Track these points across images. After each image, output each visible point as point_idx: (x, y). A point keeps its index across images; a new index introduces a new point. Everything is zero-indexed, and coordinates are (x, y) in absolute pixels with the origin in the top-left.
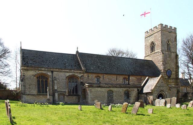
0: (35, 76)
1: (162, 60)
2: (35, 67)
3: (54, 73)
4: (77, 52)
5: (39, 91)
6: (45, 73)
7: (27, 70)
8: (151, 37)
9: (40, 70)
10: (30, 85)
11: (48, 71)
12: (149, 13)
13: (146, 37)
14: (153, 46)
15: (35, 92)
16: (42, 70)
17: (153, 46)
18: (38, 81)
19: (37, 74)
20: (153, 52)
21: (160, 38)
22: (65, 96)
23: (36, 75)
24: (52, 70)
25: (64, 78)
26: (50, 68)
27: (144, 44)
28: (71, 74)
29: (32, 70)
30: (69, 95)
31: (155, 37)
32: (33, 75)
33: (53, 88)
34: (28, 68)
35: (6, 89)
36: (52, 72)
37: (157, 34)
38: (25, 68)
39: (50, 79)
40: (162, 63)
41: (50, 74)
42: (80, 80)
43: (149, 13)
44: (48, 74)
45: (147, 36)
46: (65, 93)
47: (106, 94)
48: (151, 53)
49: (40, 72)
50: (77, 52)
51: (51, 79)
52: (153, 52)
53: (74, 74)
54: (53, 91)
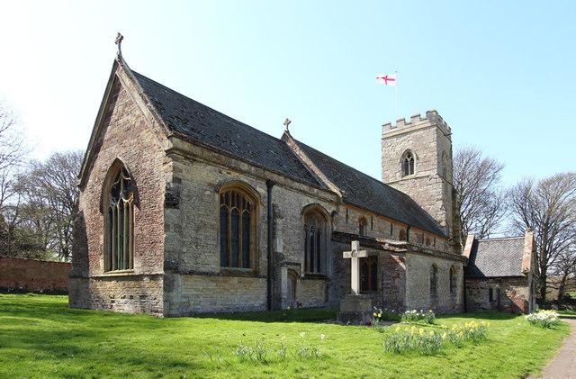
0: (216, 188)
1: (441, 197)
2: (219, 152)
3: (275, 188)
4: (287, 135)
5: (225, 261)
6: (247, 181)
7: (190, 157)
8: (402, 139)
9: (234, 169)
10: (198, 229)
11: (258, 177)
12: (394, 80)
13: (385, 136)
14: (409, 160)
15: (212, 261)
16: (241, 172)
17: (409, 160)
18: (224, 213)
19: (226, 182)
20: (410, 176)
21: (434, 144)
22: (298, 281)
23: (220, 185)
24: (269, 175)
25: (297, 212)
26: (265, 169)
27: (380, 154)
28: (312, 201)
29: (208, 162)
30: (308, 277)
31: (417, 139)
32: (210, 184)
33: (269, 248)
34: (197, 150)
35: (361, 245)
36: (270, 184)
37: (422, 132)
38: (186, 146)
39: (262, 211)
40: (440, 203)
41: (262, 190)
42: (331, 227)
43: (394, 80)
44: (258, 189)
45: (388, 136)
46: (298, 267)
47: (429, 282)
48: (405, 178)
49: (234, 175)
50: (287, 135)
51: (266, 213)
52: (407, 174)
53: (319, 202)
54: (269, 258)
